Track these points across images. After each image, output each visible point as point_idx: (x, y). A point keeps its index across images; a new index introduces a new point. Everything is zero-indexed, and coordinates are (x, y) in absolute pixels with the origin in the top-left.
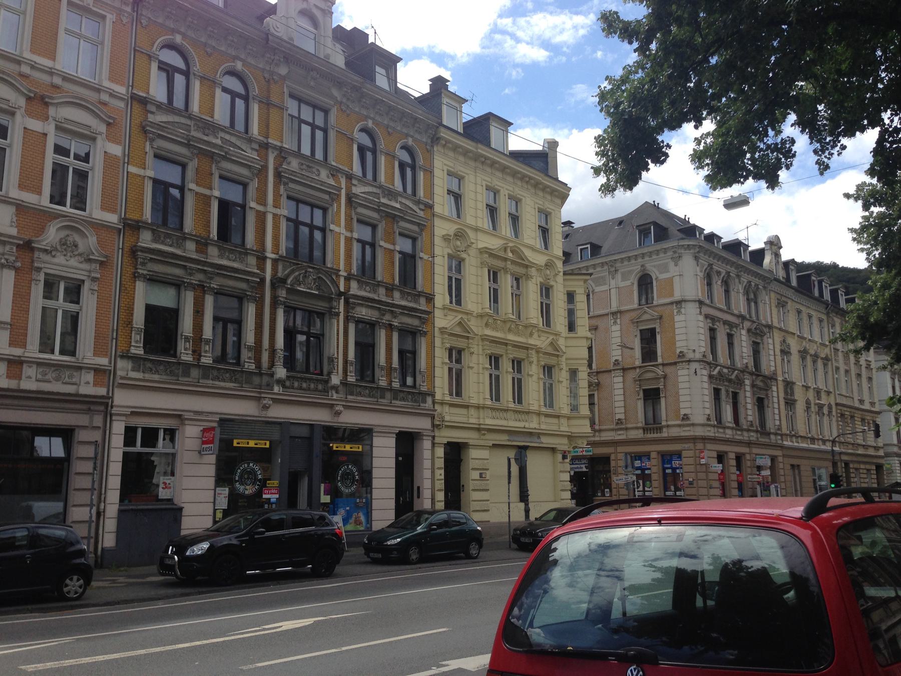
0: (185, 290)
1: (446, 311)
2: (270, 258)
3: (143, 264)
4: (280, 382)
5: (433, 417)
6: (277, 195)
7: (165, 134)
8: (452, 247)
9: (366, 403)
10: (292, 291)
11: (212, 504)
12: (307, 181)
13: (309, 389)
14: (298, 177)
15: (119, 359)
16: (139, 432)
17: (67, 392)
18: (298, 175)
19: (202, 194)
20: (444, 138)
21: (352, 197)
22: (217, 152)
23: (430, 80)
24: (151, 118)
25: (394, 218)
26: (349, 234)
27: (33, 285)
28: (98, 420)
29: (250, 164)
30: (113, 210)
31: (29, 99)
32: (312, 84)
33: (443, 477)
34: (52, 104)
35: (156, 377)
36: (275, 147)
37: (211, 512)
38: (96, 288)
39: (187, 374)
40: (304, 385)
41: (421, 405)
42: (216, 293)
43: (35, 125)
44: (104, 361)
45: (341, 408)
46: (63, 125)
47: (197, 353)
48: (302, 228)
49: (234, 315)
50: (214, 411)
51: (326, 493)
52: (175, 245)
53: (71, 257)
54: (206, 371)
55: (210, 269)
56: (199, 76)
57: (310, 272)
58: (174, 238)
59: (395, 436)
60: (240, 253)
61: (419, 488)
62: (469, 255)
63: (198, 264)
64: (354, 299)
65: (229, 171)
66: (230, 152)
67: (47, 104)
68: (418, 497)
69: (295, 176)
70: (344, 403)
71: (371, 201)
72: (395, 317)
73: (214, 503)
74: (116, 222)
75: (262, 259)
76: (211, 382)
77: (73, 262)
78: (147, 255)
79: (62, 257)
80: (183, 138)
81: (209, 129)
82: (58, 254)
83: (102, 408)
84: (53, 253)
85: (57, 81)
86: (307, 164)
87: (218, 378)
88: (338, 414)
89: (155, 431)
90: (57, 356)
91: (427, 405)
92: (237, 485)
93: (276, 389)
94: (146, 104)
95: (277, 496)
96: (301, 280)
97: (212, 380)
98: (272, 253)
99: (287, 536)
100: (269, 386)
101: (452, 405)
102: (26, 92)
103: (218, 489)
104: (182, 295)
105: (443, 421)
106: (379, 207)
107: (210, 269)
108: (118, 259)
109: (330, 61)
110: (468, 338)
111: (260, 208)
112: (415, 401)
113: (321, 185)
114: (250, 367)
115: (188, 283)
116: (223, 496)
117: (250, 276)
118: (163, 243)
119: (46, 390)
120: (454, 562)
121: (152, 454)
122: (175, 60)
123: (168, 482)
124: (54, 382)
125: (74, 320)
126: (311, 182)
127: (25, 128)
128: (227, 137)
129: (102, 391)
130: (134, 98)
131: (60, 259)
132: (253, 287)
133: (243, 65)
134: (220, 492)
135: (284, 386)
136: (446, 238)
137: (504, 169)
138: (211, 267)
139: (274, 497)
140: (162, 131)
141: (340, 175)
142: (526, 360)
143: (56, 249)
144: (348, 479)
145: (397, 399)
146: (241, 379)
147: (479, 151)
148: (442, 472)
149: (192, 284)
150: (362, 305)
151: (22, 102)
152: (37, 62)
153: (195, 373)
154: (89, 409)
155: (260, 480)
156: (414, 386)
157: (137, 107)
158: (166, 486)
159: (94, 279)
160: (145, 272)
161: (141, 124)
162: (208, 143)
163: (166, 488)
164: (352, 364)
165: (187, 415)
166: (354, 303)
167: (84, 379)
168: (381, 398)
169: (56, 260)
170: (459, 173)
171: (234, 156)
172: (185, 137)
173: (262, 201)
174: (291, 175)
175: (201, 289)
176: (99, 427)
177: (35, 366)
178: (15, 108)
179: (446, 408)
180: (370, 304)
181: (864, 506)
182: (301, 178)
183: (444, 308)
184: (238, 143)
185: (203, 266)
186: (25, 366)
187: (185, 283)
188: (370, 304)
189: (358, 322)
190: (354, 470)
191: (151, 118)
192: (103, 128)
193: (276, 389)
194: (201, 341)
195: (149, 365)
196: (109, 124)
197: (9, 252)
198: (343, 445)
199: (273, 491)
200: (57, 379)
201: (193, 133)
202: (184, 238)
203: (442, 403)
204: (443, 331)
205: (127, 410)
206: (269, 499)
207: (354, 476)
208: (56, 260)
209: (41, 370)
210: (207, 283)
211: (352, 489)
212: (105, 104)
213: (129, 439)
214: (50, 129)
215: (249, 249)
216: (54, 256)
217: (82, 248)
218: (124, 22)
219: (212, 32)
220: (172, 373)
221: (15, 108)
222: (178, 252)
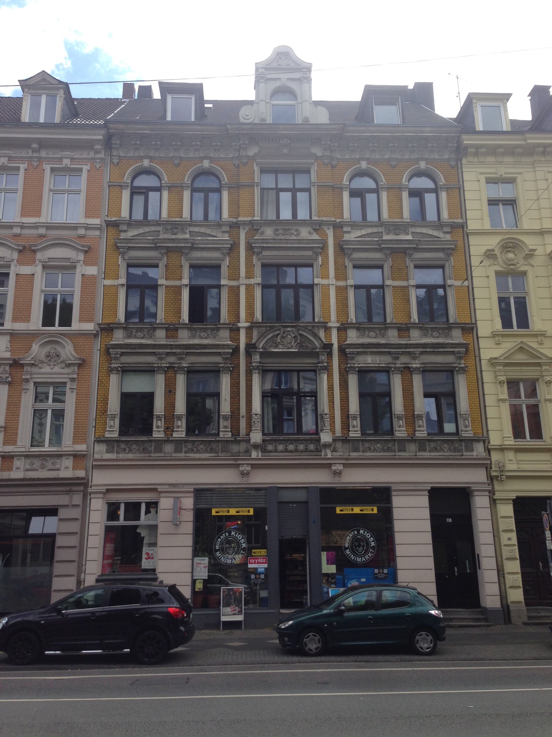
0: (457, 374)
1: (497, 338)
2: (243, 327)
3: (116, 359)
4: (256, 446)
5: (488, 468)
6: (249, 265)
7: (134, 245)
8: (501, 263)
9: (378, 459)
10: (265, 354)
11: (190, 574)
12: (282, 243)
13: (296, 451)
14: (271, 243)
15: (96, 444)
16: (122, 507)
17: (53, 477)
18: (270, 241)
19: (172, 286)
20: (472, 146)
21: (343, 245)
22: (183, 245)
23: (529, 96)
24: (123, 236)
25: (405, 253)
26: (342, 283)
27: (23, 394)
28: (77, 499)
29: (218, 246)
30: (90, 320)
31: (20, 251)
32: (285, 151)
33: (515, 541)
34: (39, 250)
35: (130, 456)
36: (245, 223)
37: (189, 582)
38: (75, 387)
39: (159, 449)
40: (291, 447)
41: (465, 453)
42: (424, 371)
43: (26, 270)
44: (82, 447)
45: (341, 467)
46: (48, 263)
47: (169, 429)
48: (373, 291)
49: (446, 389)
50: (314, 482)
51: (329, 562)
52: (147, 336)
53: (54, 365)
54: (422, 444)
55: (178, 351)
56: (167, 186)
57: (288, 331)
58: (146, 330)
59: (427, 493)
60: (212, 329)
61: (478, 555)
62: (533, 266)
63: (166, 349)
64: (350, 348)
65: (361, 259)
66: (197, 242)
67: (34, 252)
68: (480, 568)
69: (267, 243)
70: (344, 462)
71: (367, 243)
72: (414, 358)
73: (192, 572)
74: (92, 329)
75: (235, 330)
76: (429, 454)
77: (57, 369)
78: (117, 350)
79: (48, 367)
80: (150, 243)
81: (399, 229)
82: (45, 365)
83: (82, 488)
84: (40, 365)
85: (42, 231)
86: (282, 228)
87: (193, 450)
88: (338, 474)
89: (137, 505)
90: (47, 448)
91: (475, 453)
92: (218, 554)
93: (254, 454)
94: (118, 226)
95: (266, 566)
96: (279, 341)
97: (430, 452)
98: (246, 322)
99: (97, 614)
100: (248, 452)
101: (518, 450)
102: (16, 247)
103: (196, 559)
104: (456, 378)
105: (502, 471)
106: (380, 245)
107: (178, 351)
108: (96, 359)
109: (310, 123)
110: (539, 365)
111: (233, 283)
112: (456, 450)
113: (300, 243)
114: (226, 436)
115: (394, 367)
116: (202, 566)
117: (221, 349)
118: (136, 337)
119: (36, 477)
120: (360, 658)
121: (136, 527)
122: (367, 183)
123: (151, 552)
124: (40, 470)
125: (59, 415)
126: (286, 244)
127: (34, 275)
128: (419, 230)
129: (81, 473)
130: (109, 224)
131: (46, 369)
132: (226, 359)
133: (211, 162)
134: (198, 562)
135: (264, 451)
136: (490, 255)
137: (511, 151)
138: (180, 349)
139: (262, 567)
140: (130, 243)
141: (325, 228)
142: (540, 380)
143: (42, 362)
144: (359, 546)
145: (424, 450)
146: (394, 448)
147: (528, 141)
148: (514, 536)
149: (161, 367)
150: (366, 353)
151: (15, 255)
152: (89, 223)
153: (412, 447)
154: (70, 491)
155: (244, 549)
156: (457, 433)
157: (112, 230)
158: (149, 557)
159: (73, 380)
160: (418, 366)
161: (339, 243)
162: (179, 241)
163: (149, 558)
164: (355, 418)
165: (160, 489)
166: (353, 353)
167: (63, 466)
168: (399, 451)
169: (43, 370)
170: (504, 176)
171: (199, 244)
172: (152, 241)
173: (235, 276)
174: (262, 243)
175: (407, 371)
176: (79, 505)
177: (23, 458)
178: (75, 262)
179: (510, 455)
180: (374, 350)
181: (56, 617)
182: (275, 243)
183: (494, 335)
184: (208, 231)
185: (171, 349)
186: (15, 459)
187: (391, 368)
188: (374, 350)
189: (362, 372)
190: (368, 535)
191: (123, 236)
192: (81, 257)
193: (254, 454)
194: (348, 418)
195: (123, 446)
196: (86, 252)
197: (3, 372)
198: (350, 508)
199: (260, 561)
200: (43, 467)
201: (385, 237)
202: (154, 328)
203: (502, 449)
204: (493, 362)
205: (102, 488)
206: (256, 569)
207: (368, 543)
208: (43, 370)
209: (29, 461)
210: (393, 364)
211: (367, 557)
212: (19, 235)
213: (112, 514)
214: (38, 270)
215: (452, 324)
216: (40, 368)
217: (63, 356)
218: (98, 167)
219: (216, 145)
220: (145, 451)
221: (75, 262)
222: (383, 341)
